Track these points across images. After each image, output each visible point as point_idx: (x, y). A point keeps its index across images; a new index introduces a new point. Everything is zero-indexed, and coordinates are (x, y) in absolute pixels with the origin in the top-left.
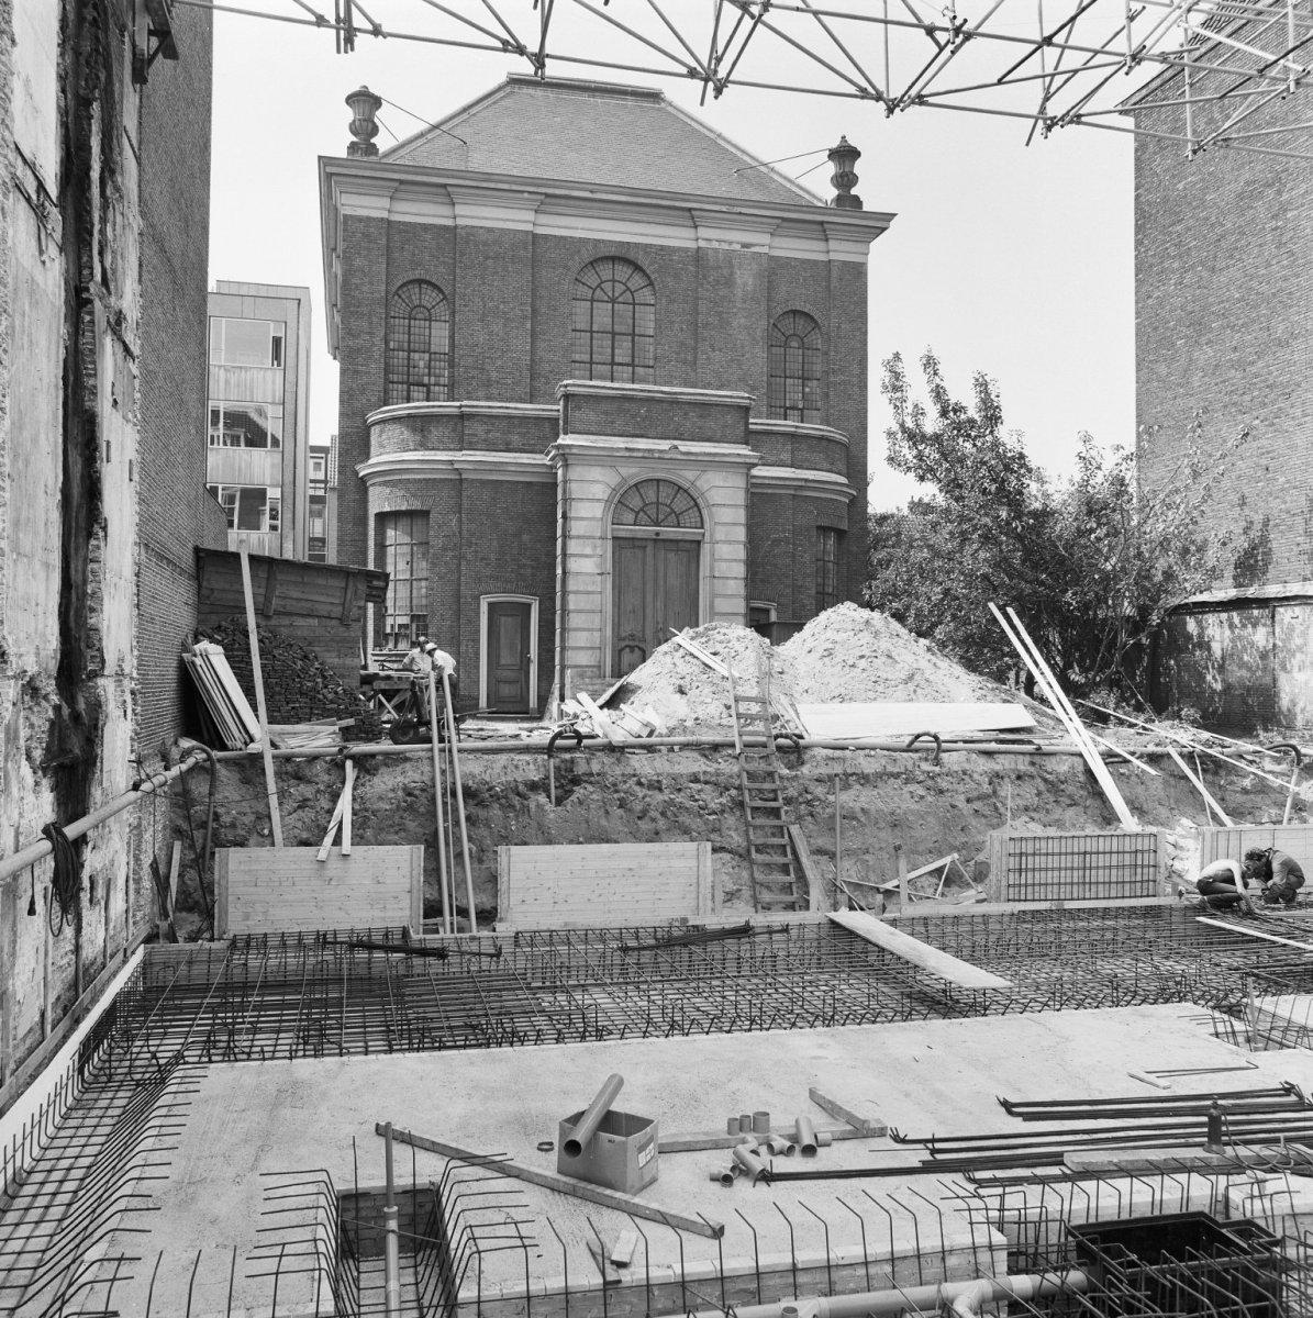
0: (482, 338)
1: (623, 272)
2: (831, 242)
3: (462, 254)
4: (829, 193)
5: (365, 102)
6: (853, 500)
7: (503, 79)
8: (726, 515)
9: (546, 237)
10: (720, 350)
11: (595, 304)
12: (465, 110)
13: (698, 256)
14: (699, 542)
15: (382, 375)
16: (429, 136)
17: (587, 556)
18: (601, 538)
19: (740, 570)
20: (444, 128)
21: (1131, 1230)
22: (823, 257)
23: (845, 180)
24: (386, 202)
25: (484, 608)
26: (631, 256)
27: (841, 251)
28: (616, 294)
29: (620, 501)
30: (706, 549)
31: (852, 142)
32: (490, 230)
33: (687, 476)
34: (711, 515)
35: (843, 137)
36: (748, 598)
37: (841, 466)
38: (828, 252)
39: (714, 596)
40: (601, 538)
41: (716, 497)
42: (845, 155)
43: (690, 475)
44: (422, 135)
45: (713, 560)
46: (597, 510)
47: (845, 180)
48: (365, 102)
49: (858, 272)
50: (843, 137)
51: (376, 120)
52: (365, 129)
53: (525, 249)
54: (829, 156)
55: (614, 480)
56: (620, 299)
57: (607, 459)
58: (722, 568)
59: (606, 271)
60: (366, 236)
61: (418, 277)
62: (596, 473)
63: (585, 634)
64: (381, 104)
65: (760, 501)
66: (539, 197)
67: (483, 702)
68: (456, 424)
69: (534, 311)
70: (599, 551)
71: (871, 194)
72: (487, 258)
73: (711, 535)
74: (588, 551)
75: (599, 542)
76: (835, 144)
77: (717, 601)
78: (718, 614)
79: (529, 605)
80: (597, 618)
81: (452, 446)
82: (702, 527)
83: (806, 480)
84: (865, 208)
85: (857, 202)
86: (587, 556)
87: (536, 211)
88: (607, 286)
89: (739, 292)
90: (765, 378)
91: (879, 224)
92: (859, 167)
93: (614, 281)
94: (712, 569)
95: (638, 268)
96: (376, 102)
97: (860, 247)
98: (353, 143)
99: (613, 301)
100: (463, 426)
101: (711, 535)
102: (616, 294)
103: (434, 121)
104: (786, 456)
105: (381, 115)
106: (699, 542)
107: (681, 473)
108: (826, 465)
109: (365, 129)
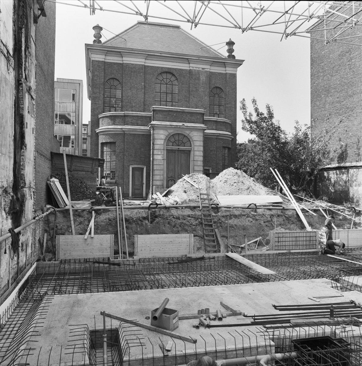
0: (130, 94)
1: (169, 76)
2: (190, 64)
4: (226, 54)
5: (98, 28)
6: (233, 139)
8: (197, 143)
9: (148, 66)
11: (161, 85)
12: (126, 31)
13: (190, 72)
15: (103, 104)
16: (116, 38)
17: (159, 155)
19: (201, 159)
20: (120, 36)
22: (224, 72)
23: (231, 51)
24: (104, 57)
25: (131, 169)
27: (229, 70)
28: (166, 82)
29: (169, 139)
30: (192, 153)
32: (132, 64)
33: (187, 132)
34: (194, 144)
35: (230, 39)
36: (204, 166)
38: (226, 71)
39: (194, 166)
41: (195, 138)
42: (231, 44)
43: (188, 132)
44: (114, 38)
45: (194, 156)
46: (162, 142)
47: (231, 51)
48: (98, 28)
50: (230, 39)
51: (101, 34)
52: (98, 36)
55: (166, 133)
56: (169, 84)
57: (165, 128)
58: (196, 158)
59: (164, 76)
60: (99, 66)
61: (112, 77)
62: (162, 132)
63: (159, 176)
65: (207, 139)
67: (130, 195)
70: (162, 153)
71: (238, 55)
72: (132, 72)
74: (160, 153)
76: (228, 41)
77: (195, 167)
79: (143, 168)
80: (162, 172)
81: (122, 124)
82: (191, 147)
83: (220, 134)
86: (159, 155)
87: (145, 59)
88: (165, 80)
89: (201, 82)
91: (240, 63)
92: (234, 47)
93: (167, 78)
94: (194, 159)
95: (173, 75)
96: (101, 29)
97: (235, 69)
98: (95, 40)
99: (167, 84)
102: (166, 82)
103: (117, 34)
104: (214, 127)
105: (102, 32)
107: (185, 132)
109: (98, 36)
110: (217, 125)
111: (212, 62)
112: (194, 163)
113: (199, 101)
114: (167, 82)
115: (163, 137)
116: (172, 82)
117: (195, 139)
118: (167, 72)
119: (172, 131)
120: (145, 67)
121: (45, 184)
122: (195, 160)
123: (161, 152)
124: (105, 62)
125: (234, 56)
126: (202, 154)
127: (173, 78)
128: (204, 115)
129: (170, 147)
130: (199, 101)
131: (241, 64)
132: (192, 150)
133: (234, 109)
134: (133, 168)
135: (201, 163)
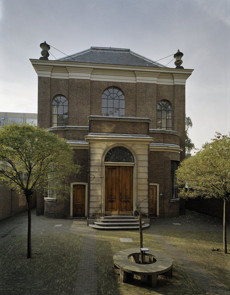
1: (116, 91)
3: (71, 87)
5: (45, 47)
6: (181, 152)
7: (90, 48)
10: (143, 111)
13: (137, 84)
14: (133, 167)
15: (49, 121)
18: (101, 166)
19: (146, 176)
21: (137, 58)
22: (135, 82)
23: (178, 63)
24: (89, 75)
25: (72, 186)
26: (120, 87)
27: (178, 82)
29: (108, 156)
30: (135, 169)
31: (180, 51)
34: (137, 158)
35: (179, 50)
36: (149, 181)
37: (178, 143)
39: (138, 184)
40: (101, 166)
41: (138, 152)
42: (179, 55)
47: (178, 63)
48: (45, 47)
49: (183, 87)
50: (179, 50)
51: (48, 52)
52: (45, 54)
53: (88, 85)
54: (174, 57)
58: (140, 175)
59: (111, 90)
61: (59, 93)
64: (49, 48)
65: (152, 155)
66: (91, 69)
67: (71, 214)
68: (64, 133)
69: (91, 102)
70: (100, 170)
72: (78, 88)
73: (137, 164)
74: (97, 170)
75: (100, 167)
76: (176, 52)
77: (139, 186)
78: (139, 190)
79: (85, 185)
82: (134, 162)
84: (184, 68)
85: (182, 68)
90: (156, 119)
91: (188, 73)
92: (183, 59)
93: (113, 93)
94: (137, 175)
95: (120, 90)
96: (48, 47)
97: (183, 80)
98: (41, 57)
99: (113, 99)
100: (66, 133)
101: (137, 164)
104: (161, 140)
105: (50, 51)
106: (133, 167)
108: (174, 142)
109: (45, 54)
110: (164, 137)
111: (159, 73)
112: (137, 181)
113: (146, 114)
114: (114, 98)
115: (101, 152)
116: (118, 97)
117: (139, 153)
118: (114, 87)
119: (111, 144)
120: (92, 82)
121: (146, 152)
122: (139, 177)
123: (99, 169)
124: (51, 79)
125: (182, 67)
126: (146, 170)
127: (120, 93)
128: (151, 125)
129: (110, 163)
130: (146, 114)
131: (190, 74)
132: (136, 165)
133: (182, 121)
134: (74, 185)
135: (145, 181)
